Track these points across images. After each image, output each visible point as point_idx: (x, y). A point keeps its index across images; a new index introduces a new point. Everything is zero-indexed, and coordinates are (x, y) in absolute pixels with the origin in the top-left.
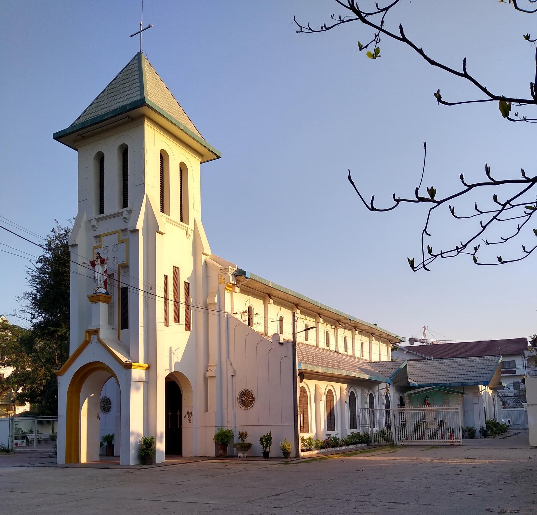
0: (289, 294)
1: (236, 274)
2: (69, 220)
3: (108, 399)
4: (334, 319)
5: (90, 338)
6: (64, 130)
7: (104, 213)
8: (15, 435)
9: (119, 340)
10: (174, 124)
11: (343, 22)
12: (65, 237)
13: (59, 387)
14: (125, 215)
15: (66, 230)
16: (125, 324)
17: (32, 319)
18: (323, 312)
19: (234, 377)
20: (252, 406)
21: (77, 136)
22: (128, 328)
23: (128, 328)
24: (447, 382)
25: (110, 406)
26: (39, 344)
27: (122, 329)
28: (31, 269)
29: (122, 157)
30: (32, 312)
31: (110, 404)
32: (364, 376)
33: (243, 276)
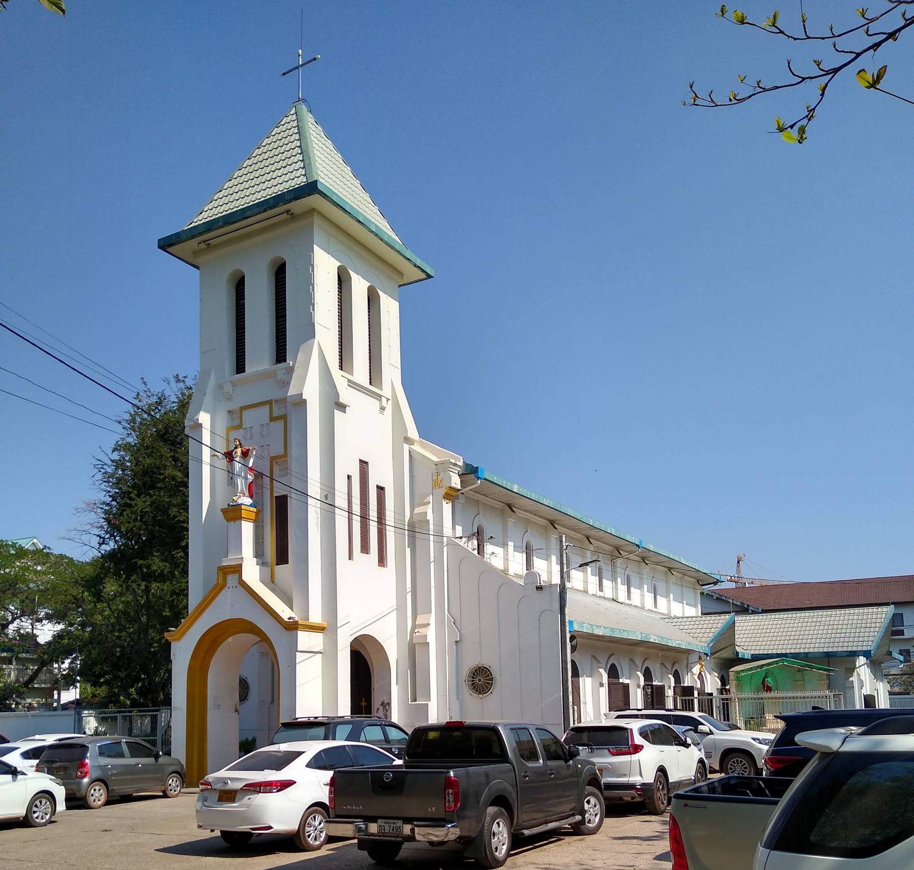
0: (543, 504)
1: (461, 471)
2: (165, 379)
3: (243, 679)
4: (611, 545)
5: (225, 580)
6: (177, 233)
7: (245, 372)
8: (156, 738)
9: (273, 582)
10: (362, 223)
11: (765, 90)
12: (158, 408)
13: (173, 661)
14: (281, 375)
15: (160, 396)
16: (282, 557)
17: (100, 544)
18: (594, 534)
19: (459, 644)
20: (489, 692)
21: (199, 244)
22: (288, 563)
23: (288, 563)
24: (802, 651)
25: (248, 692)
26: (111, 587)
27: (277, 565)
28: (102, 461)
29: (273, 278)
30: (100, 533)
31: (248, 688)
32: (668, 642)
33: (473, 475)
